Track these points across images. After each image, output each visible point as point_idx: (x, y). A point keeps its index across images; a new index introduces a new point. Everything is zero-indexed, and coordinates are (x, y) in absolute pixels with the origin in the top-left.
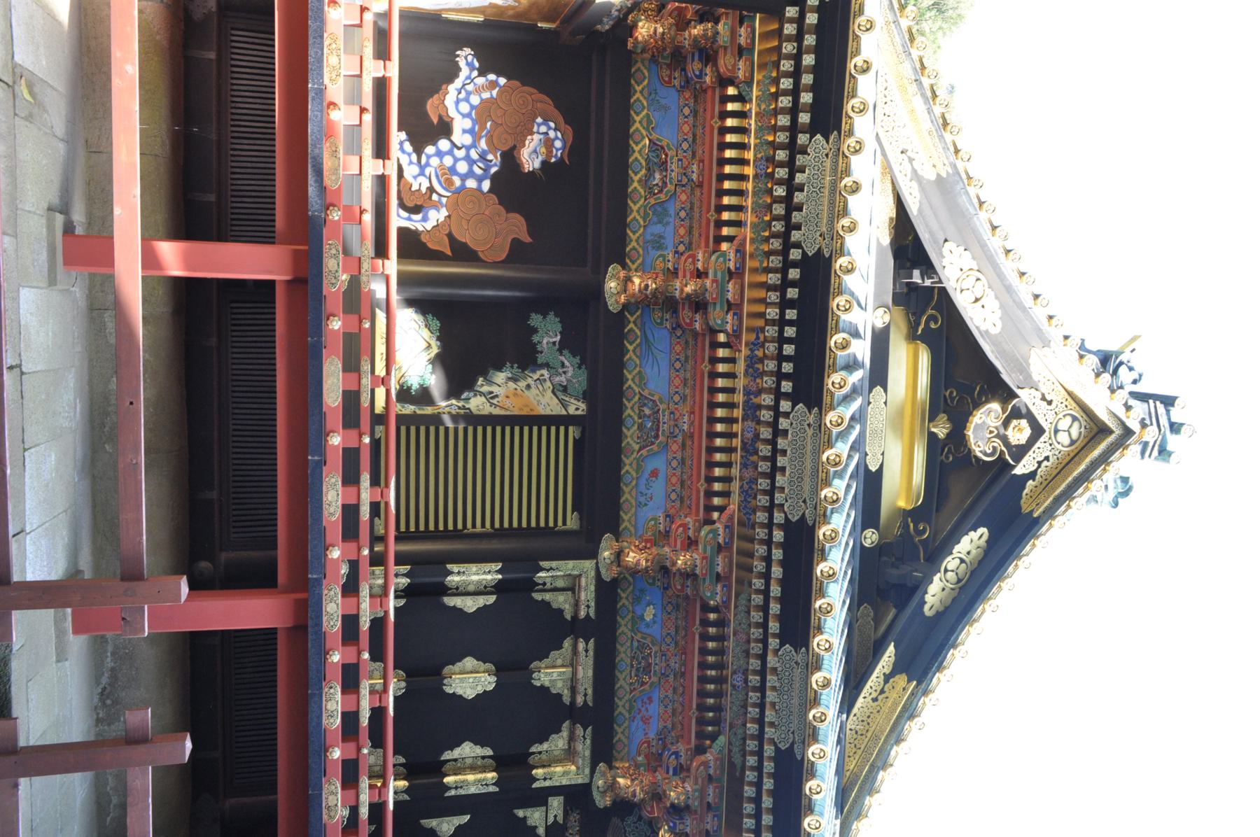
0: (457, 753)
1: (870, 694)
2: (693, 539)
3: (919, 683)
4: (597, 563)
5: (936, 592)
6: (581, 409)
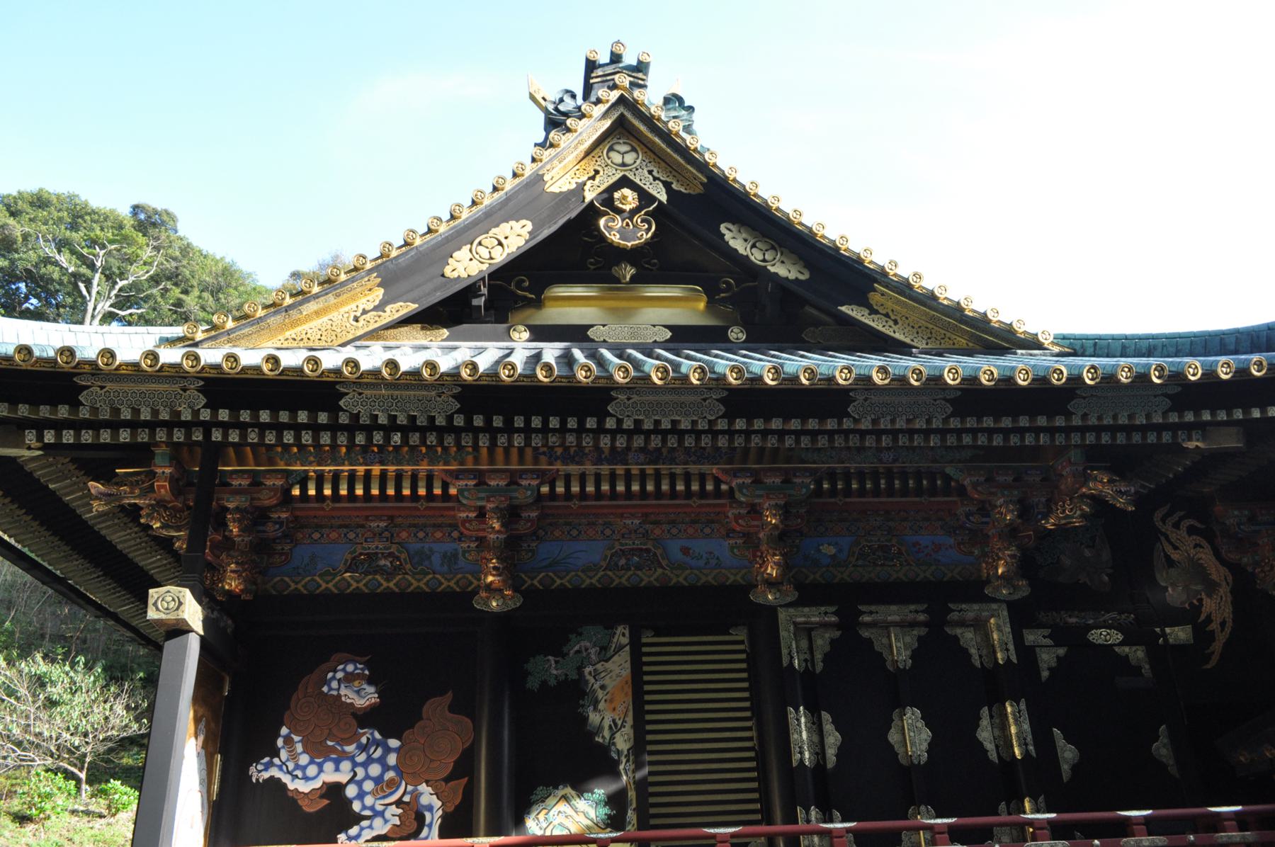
0: (989, 747)
1: (890, 327)
2: (749, 509)
3: (876, 281)
4: (781, 606)
5: (784, 269)
6: (623, 630)
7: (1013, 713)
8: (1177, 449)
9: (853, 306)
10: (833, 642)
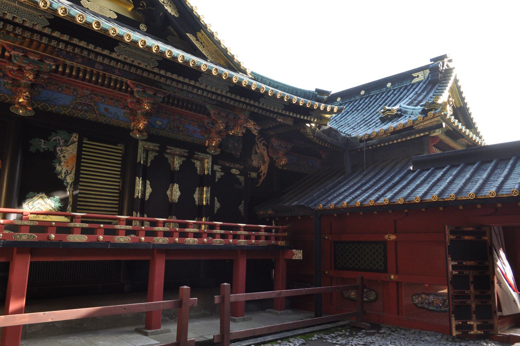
0: (196, 200)
2: (137, 100)
3: (202, 29)
4: (140, 140)
6: (76, 136)
7: (206, 191)
8: (275, 120)
9: (191, 35)
10: (155, 157)
